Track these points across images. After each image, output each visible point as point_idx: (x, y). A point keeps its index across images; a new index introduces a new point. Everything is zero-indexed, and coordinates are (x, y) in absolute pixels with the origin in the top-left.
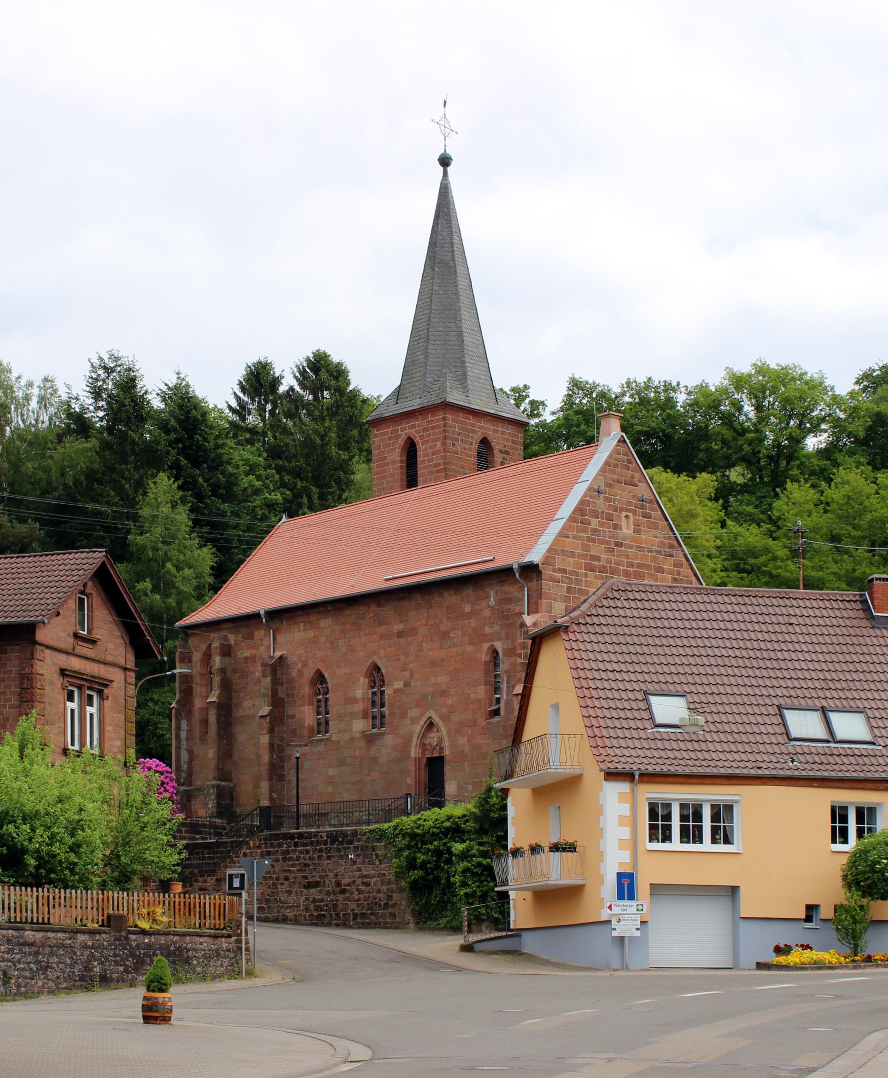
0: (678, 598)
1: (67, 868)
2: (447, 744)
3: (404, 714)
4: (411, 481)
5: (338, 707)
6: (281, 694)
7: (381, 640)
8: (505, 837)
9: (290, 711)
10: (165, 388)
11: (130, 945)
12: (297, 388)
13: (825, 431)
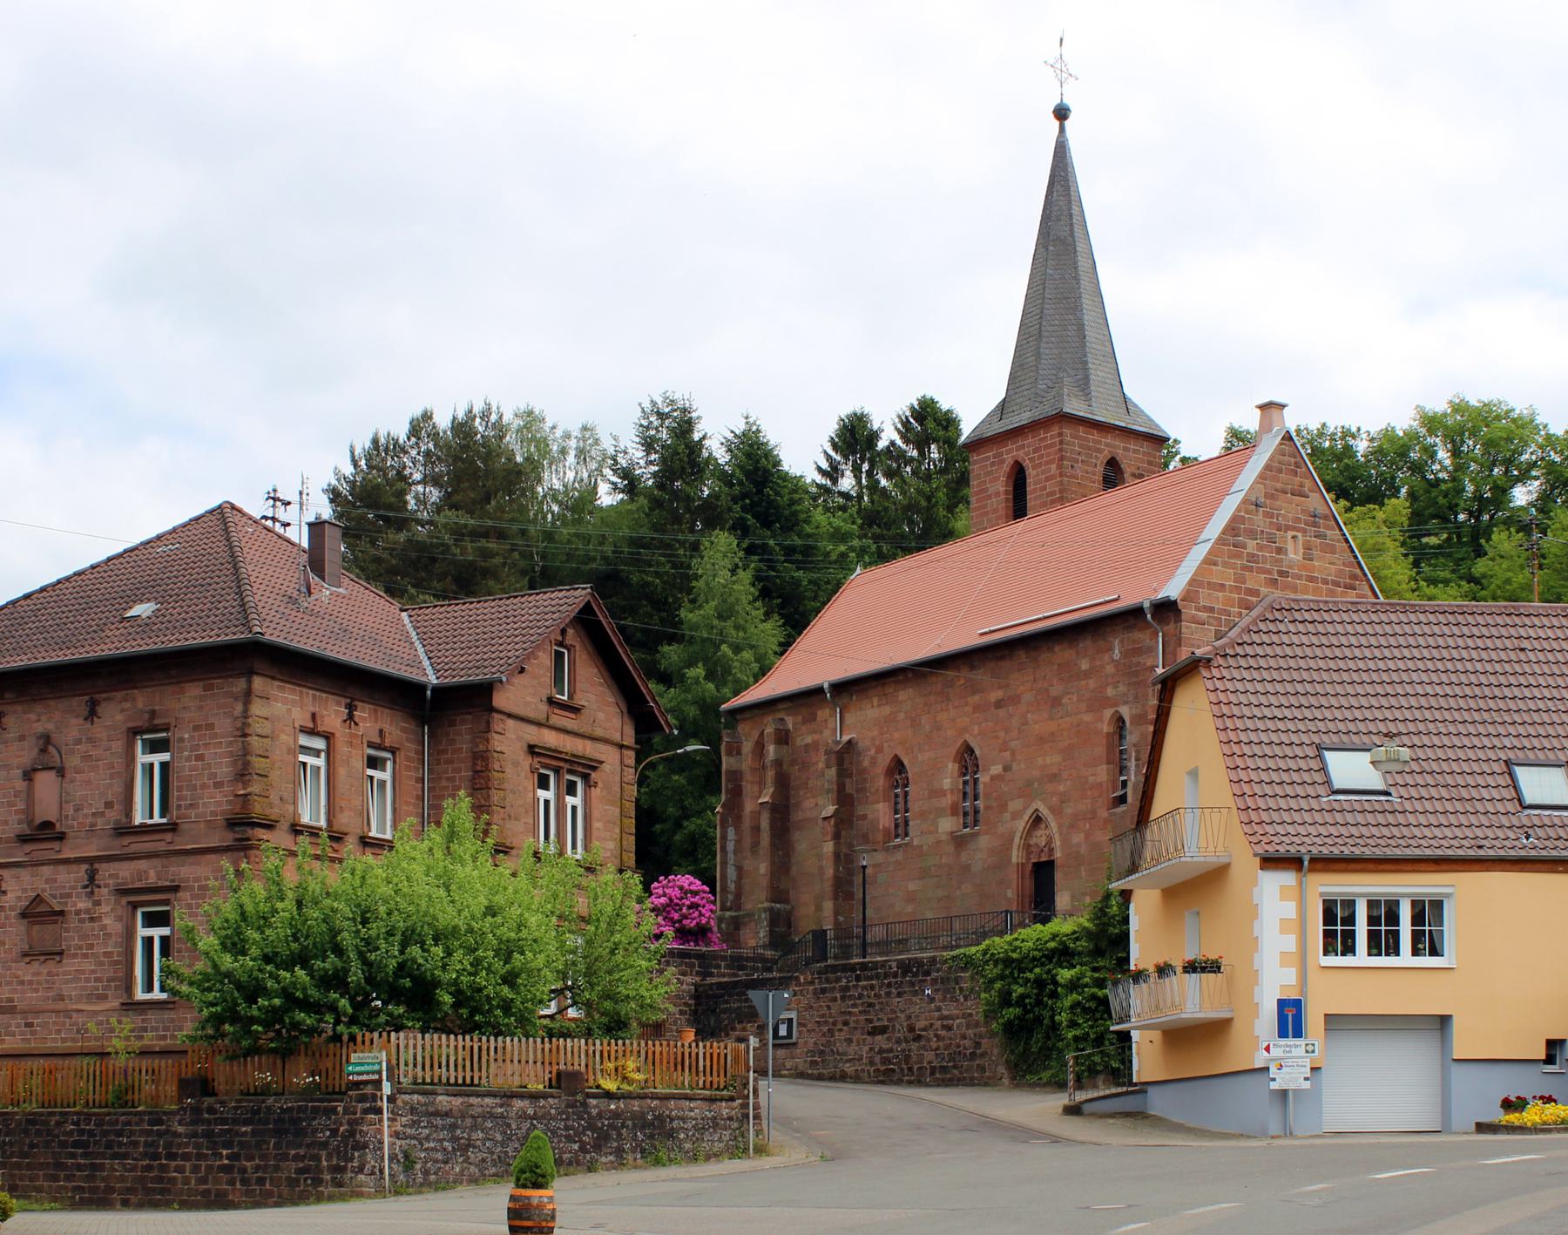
0: (1364, 617)
1: (498, 1007)
3: (1003, 807)
4: (1019, 509)
6: (849, 789)
8: (1127, 960)
9: (860, 811)
10: (730, 436)
11: (589, 1114)
12: (899, 442)
13: (1536, 478)
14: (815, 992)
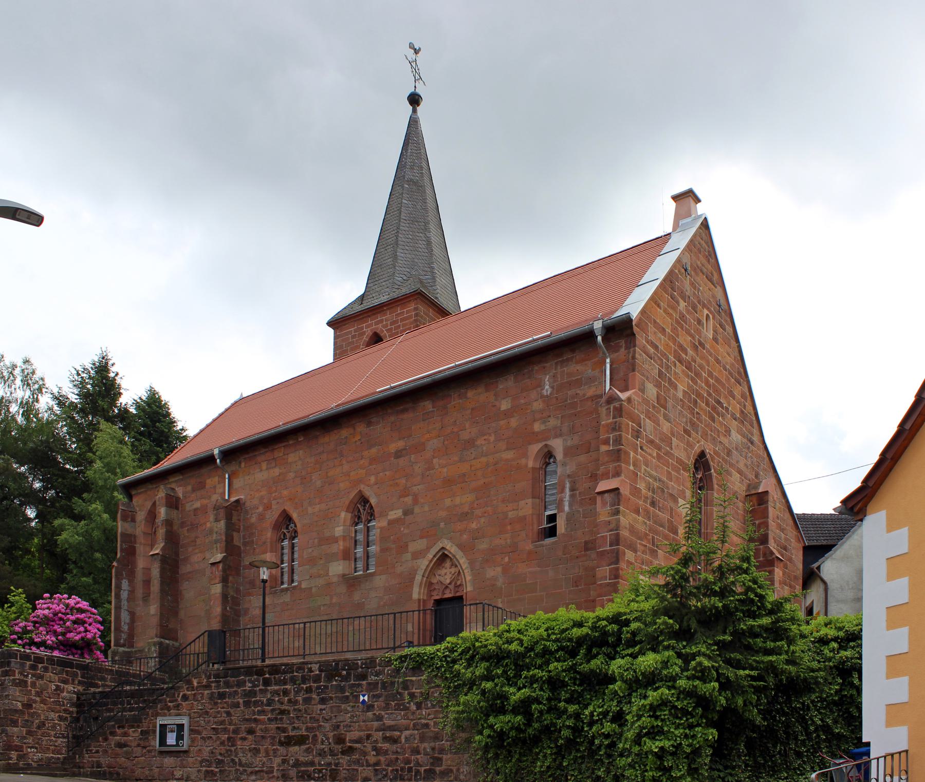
5: (310, 550)
6: (237, 540)
7: (370, 464)
14: (211, 697)
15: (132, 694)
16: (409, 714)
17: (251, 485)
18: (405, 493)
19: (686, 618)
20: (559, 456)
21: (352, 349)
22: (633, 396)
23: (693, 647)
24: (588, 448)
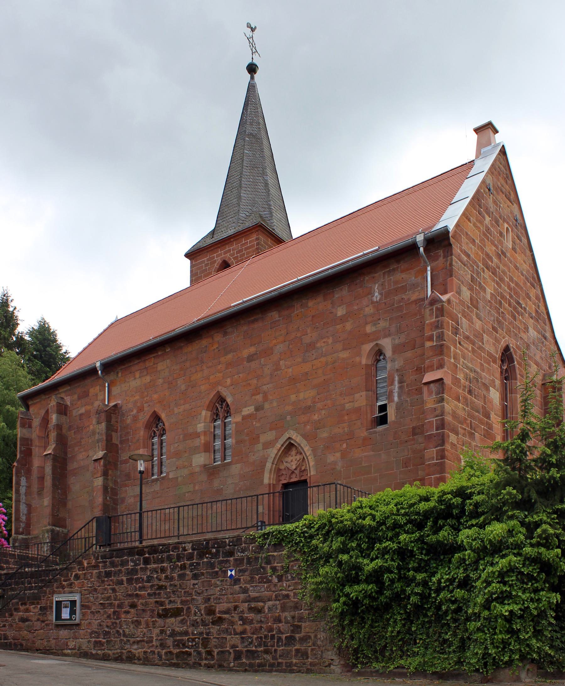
2: (312, 463)
5: (176, 445)
6: (116, 440)
7: (227, 368)
14: (99, 576)
15: (32, 575)
16: (272, 586)
17: (126, 392)
18: (256, 392)
19: (526, 489)
20: (388, 353)
21: (205, 276)
22: (452, 298)
23: (535, 516)
24: (412, 345)
